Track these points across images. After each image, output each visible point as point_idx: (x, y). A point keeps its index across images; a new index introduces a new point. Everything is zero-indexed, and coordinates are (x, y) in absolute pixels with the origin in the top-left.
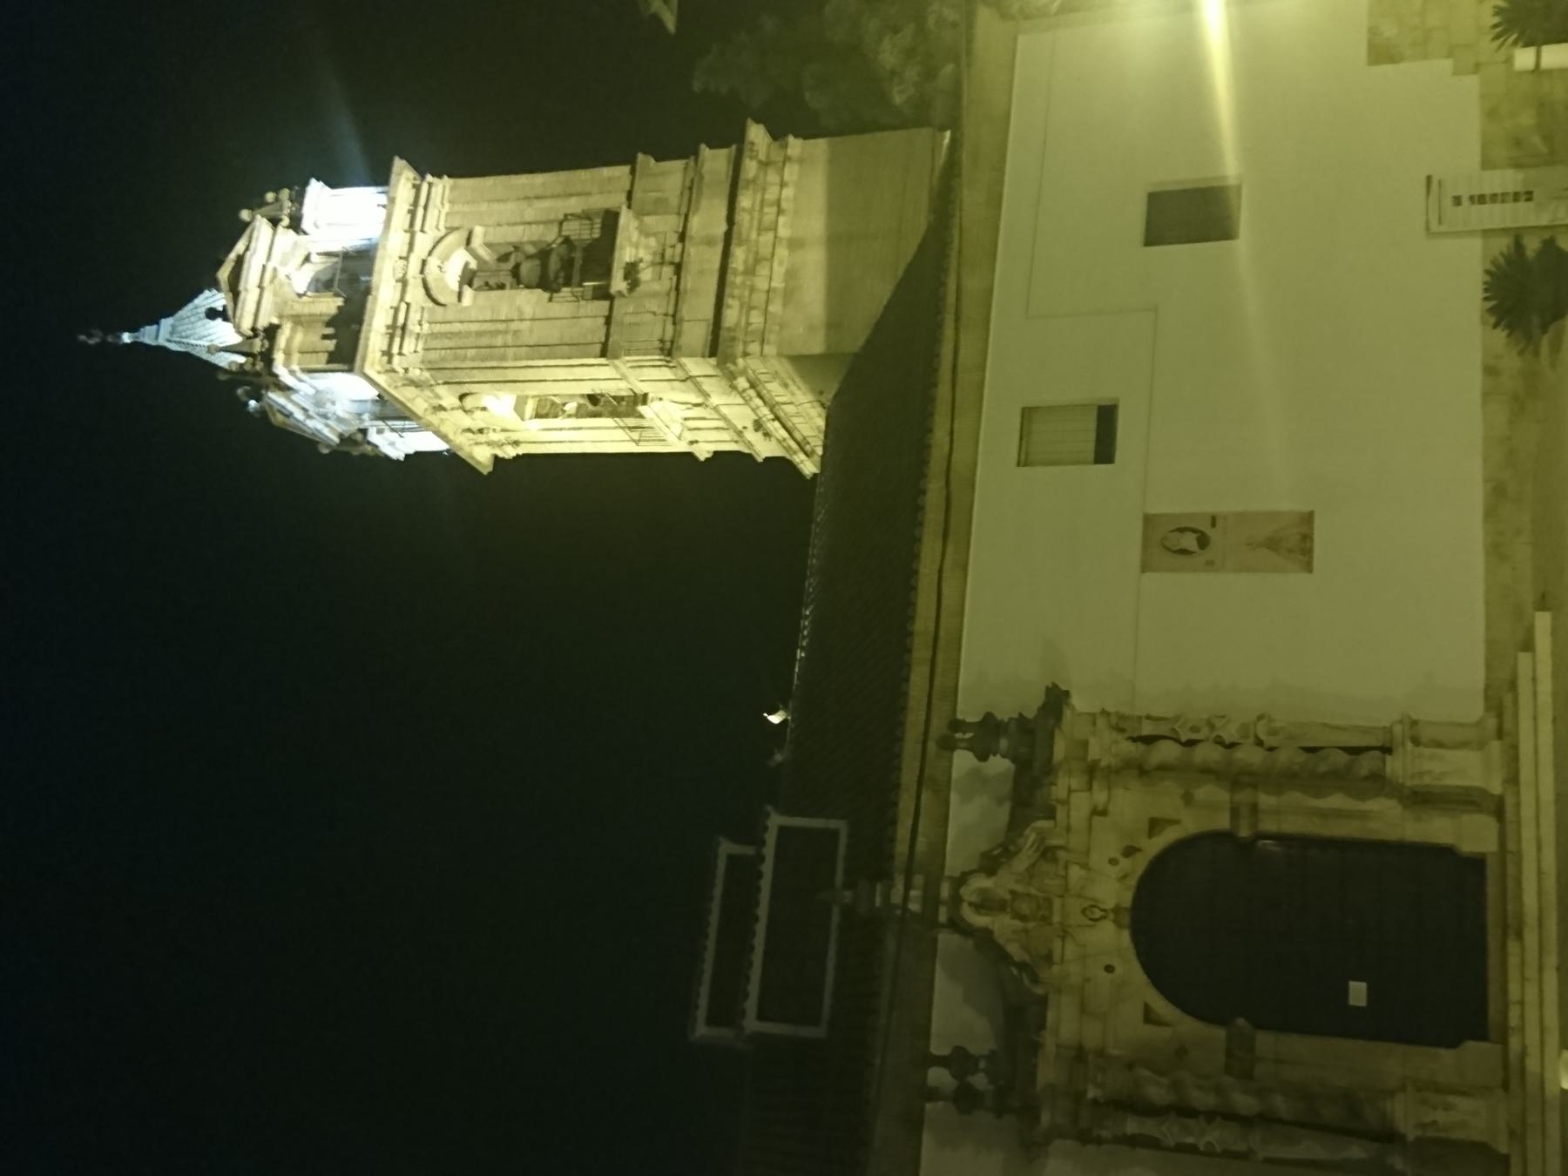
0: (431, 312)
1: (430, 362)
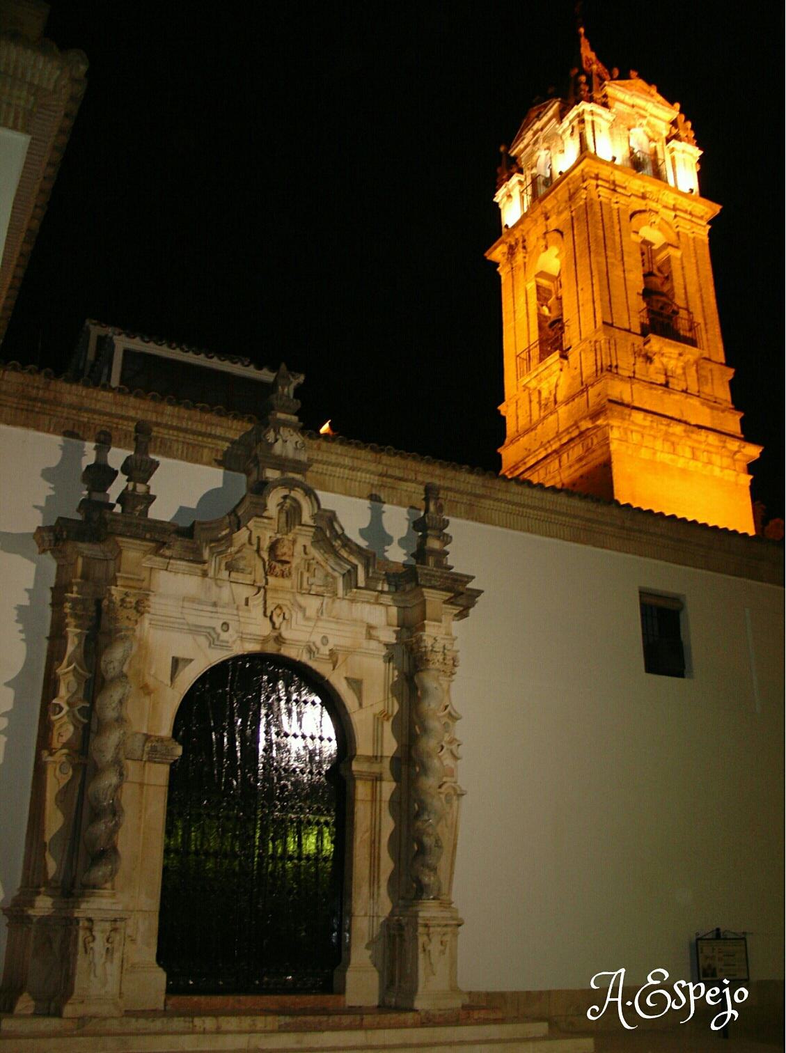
0: (626, 211)
1: (592, 205)
